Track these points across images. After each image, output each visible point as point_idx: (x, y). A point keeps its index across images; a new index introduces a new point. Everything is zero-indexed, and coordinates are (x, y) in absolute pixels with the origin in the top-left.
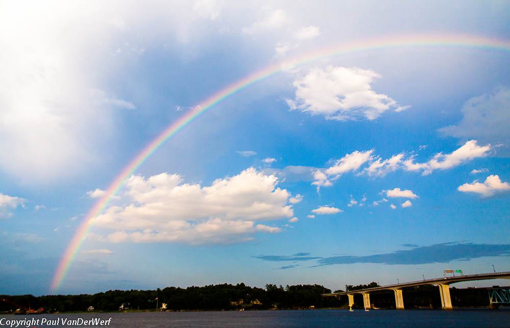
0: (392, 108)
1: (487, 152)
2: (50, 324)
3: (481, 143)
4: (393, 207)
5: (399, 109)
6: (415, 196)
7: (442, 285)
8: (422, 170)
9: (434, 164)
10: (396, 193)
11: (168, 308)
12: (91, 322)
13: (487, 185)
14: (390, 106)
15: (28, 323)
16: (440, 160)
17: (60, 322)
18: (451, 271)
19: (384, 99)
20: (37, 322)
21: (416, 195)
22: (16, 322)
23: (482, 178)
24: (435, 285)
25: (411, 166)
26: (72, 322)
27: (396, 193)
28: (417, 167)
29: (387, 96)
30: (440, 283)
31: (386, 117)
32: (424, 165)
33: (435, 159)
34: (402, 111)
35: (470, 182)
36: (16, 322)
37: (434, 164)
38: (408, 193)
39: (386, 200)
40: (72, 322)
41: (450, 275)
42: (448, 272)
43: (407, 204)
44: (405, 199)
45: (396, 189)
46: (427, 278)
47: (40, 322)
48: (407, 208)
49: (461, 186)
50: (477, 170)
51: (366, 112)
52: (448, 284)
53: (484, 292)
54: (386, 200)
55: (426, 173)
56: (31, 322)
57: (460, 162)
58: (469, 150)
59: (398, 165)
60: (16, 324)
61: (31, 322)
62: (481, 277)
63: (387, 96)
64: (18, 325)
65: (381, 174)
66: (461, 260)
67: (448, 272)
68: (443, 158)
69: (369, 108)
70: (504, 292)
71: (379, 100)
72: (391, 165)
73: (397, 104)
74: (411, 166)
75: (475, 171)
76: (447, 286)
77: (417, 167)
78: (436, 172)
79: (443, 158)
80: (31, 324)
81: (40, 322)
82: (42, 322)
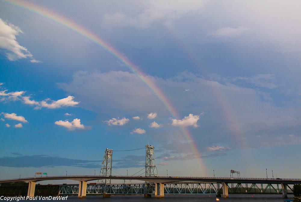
0: (29, 58)
1: (76, 105)
2: (46, 198)
3: (74, 100)
4: (8, 125)
5: (34, 61)
6: (26, 121)
7: (31, 182)
8: (35, 106)
9: (44, 104)
10: (13, 116)
11: (75, 187)
12: (56, 198)
13: (73, 124)
14: (28, 57)
15: (18, 199)
16: (49, 102)
17: (38, 198)
18: (40, 173)
19: (24, 51)
20: (23, 198)
21: (27, 121)
22: (10, 198)
23: (71, 120)
24: (27, 182)
25: (28, 101)
26: (45, 198)
27: (13, 116)
28: (32, 102)
29: (27, 49)
30: (31, 181)
31: (22, 63)
32: (37, 103)
33: (46, 101)
34: (35, 63)
35: (64, 120)
36: (10, 198)
37: (44, 104)
38: (21, 118)
39: (3, 120)
40: (45, 198)
41: (39, 176)
42: (38, 173)
43: (20, 125)
44: (18, 122)
45: (14, 113)
46: (23, 177)
47: (25, 198)
48: (18, 128)
49: (57, 122)
50: (69, 113)
51: (9, 54)
52: (36, 181)
53: (57, 187)
54: (3, 120)
55: (37, 108)
56: (20, 198)
57: (60, 107)
58: (68, 101)
59: (18, 98)
60: (10, 199)
61: (20, 198)
62: (59, 178)
63: (27, 49)
64: (12, 199)
65: (4, 101)
66: (49, 167)
67: (38, 173)
68: (51, 102)
69: (12, 52)
70: (68, 188)
71: (20, 50)
72: (13, 96)
73: (33, 57)
74: (28, 101)
75: (67, 114)
76: (35, 183)
77: (32, 102)
78: (45, 109)
79: (51, 102)
80: (20, 199)
81: (25, 198)
82: (27, 198)
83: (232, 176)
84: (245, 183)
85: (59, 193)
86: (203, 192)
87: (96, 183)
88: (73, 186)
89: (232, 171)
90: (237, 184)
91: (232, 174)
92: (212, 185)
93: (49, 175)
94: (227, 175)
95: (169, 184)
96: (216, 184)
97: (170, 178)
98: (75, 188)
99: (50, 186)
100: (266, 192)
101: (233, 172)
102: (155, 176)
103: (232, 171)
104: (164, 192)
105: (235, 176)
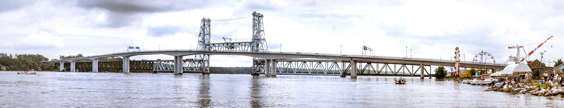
83: (364, 54)
84: (411, 65)
85: (154, 69)
86: (294, 71)
87: (193, 59)
88: (161, 62)
89: (457, 48)
90: (367, 63)
91: (364, 51)
92: (193, 63)
93: (142, 50)
94: (358, 52)
95: (281, 61)
96: (341, 63)
97: (298, 55)
98: (163, 64)
99: (145, 62)
100: (381, 73)
101: (365, 48)
102: (265, 51)
103: (365, 47)
104: (75, 68)
105: (368, 54)
